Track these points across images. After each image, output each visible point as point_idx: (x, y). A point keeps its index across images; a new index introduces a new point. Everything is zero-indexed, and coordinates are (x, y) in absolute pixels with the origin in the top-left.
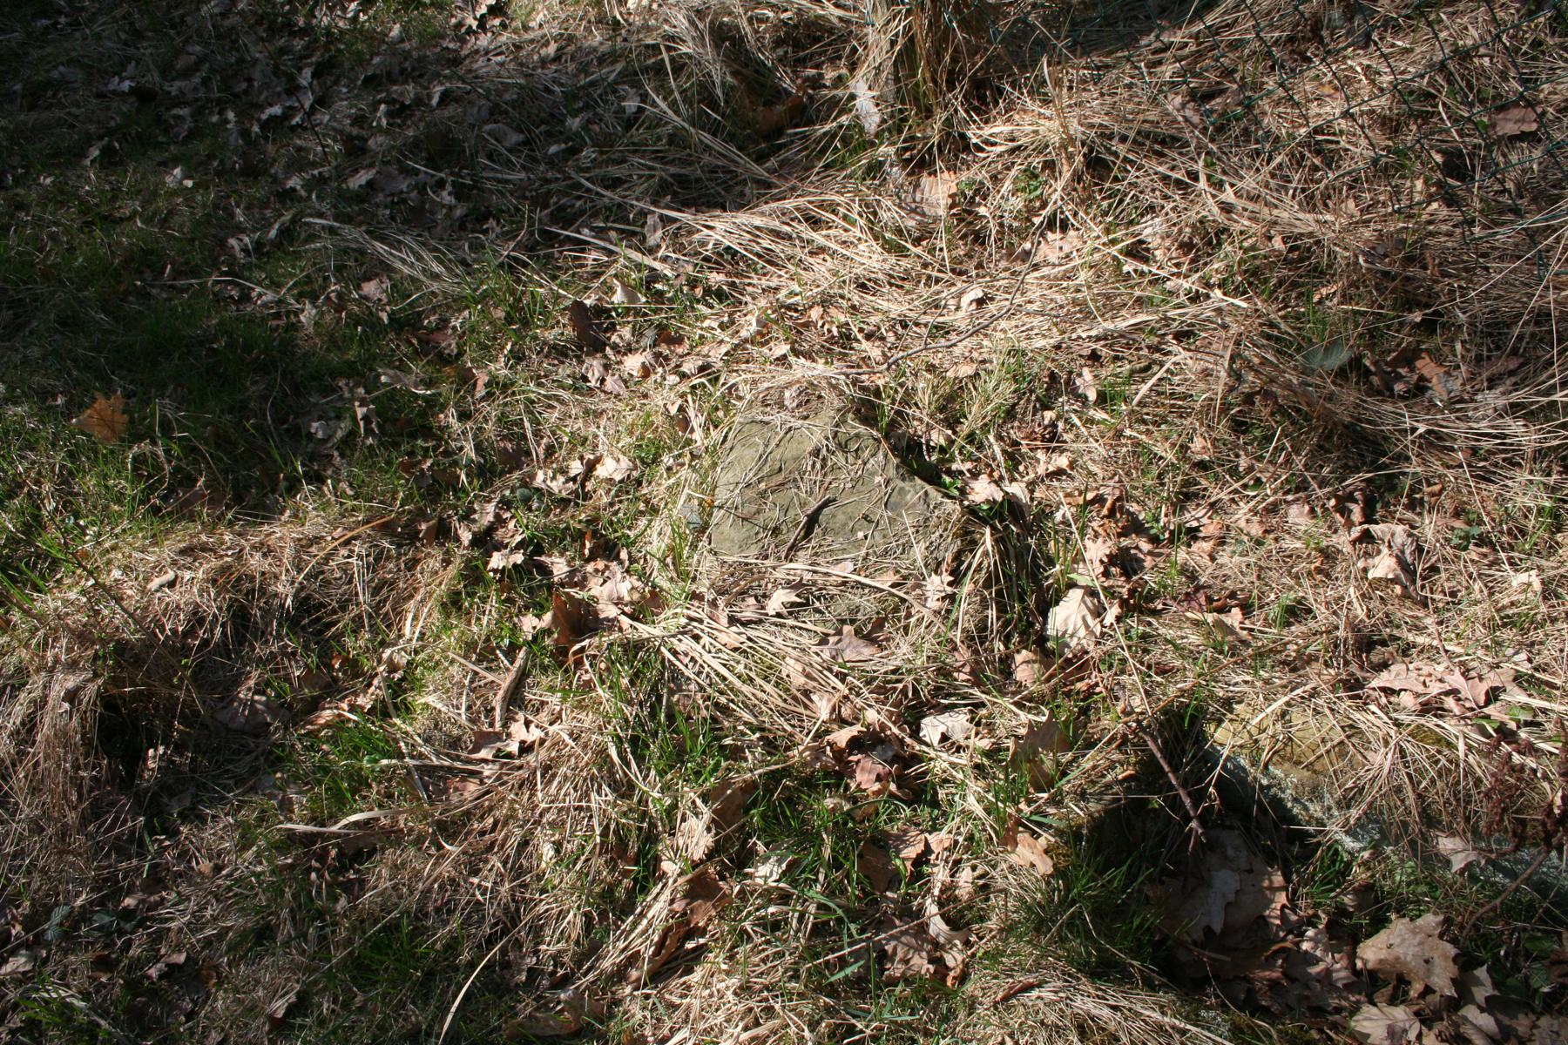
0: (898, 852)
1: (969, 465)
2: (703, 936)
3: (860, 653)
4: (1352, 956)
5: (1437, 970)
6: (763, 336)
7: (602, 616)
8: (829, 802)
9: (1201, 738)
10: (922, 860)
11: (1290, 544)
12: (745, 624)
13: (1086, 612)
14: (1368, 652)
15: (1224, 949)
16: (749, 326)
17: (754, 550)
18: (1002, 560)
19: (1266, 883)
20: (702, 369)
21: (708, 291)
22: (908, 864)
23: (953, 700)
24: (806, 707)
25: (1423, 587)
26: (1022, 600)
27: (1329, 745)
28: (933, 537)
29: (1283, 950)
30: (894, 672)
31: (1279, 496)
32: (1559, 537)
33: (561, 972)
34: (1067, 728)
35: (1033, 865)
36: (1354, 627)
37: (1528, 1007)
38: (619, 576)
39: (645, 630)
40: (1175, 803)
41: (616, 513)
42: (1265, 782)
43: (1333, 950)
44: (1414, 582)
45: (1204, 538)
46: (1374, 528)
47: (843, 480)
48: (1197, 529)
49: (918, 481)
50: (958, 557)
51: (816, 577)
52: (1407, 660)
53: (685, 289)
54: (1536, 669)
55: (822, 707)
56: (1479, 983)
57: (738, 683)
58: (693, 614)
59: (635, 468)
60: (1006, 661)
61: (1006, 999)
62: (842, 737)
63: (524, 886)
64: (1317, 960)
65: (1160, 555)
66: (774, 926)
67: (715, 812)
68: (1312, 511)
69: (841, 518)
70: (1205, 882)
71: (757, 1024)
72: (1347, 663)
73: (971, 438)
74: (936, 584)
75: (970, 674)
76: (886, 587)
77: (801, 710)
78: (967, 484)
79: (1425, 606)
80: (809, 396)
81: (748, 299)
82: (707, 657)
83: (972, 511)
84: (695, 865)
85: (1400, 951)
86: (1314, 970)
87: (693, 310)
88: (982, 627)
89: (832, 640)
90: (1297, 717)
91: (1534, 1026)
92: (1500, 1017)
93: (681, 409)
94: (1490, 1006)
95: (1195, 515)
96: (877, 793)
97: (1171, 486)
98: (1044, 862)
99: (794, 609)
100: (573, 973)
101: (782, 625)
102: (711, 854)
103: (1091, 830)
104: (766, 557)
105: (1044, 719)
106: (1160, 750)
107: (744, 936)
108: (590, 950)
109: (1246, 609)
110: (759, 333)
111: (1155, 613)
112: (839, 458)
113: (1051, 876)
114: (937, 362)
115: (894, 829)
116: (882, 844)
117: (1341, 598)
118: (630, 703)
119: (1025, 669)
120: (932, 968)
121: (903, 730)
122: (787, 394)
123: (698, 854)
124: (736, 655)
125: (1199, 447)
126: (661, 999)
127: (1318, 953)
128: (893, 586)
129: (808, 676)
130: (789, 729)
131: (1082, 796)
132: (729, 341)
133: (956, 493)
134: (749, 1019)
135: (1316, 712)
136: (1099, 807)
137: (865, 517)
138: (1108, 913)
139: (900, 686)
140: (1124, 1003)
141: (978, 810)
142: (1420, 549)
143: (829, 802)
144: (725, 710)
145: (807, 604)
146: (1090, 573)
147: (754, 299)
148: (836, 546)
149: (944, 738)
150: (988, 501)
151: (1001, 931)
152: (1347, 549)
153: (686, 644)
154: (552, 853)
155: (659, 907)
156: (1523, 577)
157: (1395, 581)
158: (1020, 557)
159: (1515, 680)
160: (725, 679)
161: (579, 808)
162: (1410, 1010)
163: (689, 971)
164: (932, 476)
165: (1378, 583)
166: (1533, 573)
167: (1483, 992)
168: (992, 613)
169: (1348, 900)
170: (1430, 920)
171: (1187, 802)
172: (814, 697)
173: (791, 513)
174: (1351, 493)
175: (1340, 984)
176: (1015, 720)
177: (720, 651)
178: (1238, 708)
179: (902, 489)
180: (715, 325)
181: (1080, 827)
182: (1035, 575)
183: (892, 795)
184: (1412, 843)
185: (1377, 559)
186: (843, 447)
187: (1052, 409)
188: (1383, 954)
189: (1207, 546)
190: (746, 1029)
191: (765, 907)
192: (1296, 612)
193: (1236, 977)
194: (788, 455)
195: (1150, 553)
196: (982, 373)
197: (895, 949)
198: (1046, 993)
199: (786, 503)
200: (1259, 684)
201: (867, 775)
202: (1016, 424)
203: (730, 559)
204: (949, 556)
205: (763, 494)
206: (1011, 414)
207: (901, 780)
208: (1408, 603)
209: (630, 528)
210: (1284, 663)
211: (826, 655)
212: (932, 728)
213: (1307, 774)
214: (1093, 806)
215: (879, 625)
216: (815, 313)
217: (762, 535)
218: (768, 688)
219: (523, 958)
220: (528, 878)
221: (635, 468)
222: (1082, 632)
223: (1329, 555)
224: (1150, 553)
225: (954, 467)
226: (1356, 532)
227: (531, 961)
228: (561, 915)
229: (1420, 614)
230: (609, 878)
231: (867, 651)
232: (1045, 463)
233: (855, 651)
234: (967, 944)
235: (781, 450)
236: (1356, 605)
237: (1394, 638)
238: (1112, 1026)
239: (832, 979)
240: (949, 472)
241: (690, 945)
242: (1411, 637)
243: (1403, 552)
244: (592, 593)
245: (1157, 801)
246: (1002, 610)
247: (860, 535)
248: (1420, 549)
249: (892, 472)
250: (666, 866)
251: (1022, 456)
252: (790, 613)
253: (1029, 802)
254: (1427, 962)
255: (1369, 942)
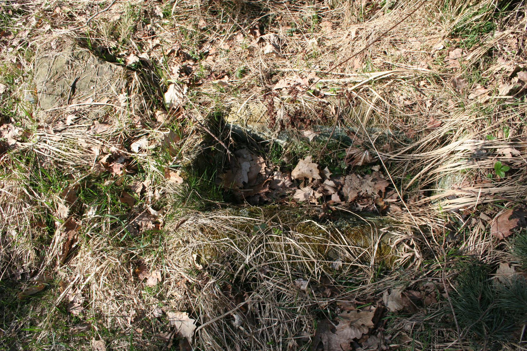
0: (135, 191)
1: (125, 52)
2: (76, 241)
3: (103, 129)
4: (290, 176)
5: (314, 173)
6: (40, 24)
7: (10, 144)
8: (107, 183)
9: (223, 122)
10: (143, 191)
11: (239, 49)
12: (60, 132)
13: (176, 91)
14: (271, 78)
15: (251, 187)
16: (34, 22)
17: (57, 104)
18: (143, 82)
19: (258, 162)
20: (20, 42)
21: (14, 12)
22: (139, 194)
23: (140, 135)
24: (91, 153)
25: (283, 52)
26: (154, 94)
27: (263, 113)
28: (117, 81)
29: (268, 181)
30: (116, 132)
31: (232, 34)
32: (321, 25)
33: (33, 271)
34: (178, 132)
35: (177, 182)
36: (265, 72)
37: (341, 175)
38: (14, 128)
39: (26, 145)
40: (220, 146)
41: (5, 106)
42: (248, 130)
43: (283, 176)
44: (279, 51)
45: (210, 55)
46: (263, 37)
47: (80, 70)
48: (208, 52)
49: (107, 62)
50: (127, 86)
51: (81, 107)
52: (284, 77)
53: (5, 13)
54: (322, 70)
55: (96, 151)
56: (327, 172)
57: (64, 153)
58: (41, 134)
59: (7, 87)
60: (153, 116)
61: (177, 227)
62: (104, 160)
63: (9, 247)
64: (280, 181)
65: (197, 65)
66: (98, 230)
67: (66, 199)
68: (244, 36)
69: (83, 84)
70: (239, 168)
71: (101, 264)
72: (265, 84)
73: (124, 42)
74: (122, 97)
75: (141, 124)
76: (105, 103)
77: (89, 155)
78: (126, 59)
79: (285, 58)
80: (60, 43)
81: (32, 11)
82: (50, 147)
83: (129, 68)
84: (66, 219)
85: (302, 170)
86: (279, 184)
87: (11, 20)
88: (142, 107)
89: (92, 127)
90: (251, 106)
91: (345, 180)
92: (335, 180)
93: (17, 60)
94: (331, 178)
95: (206, 47)
96: (122, 174)
97: (195, 41)
98: (180, 180)
99: (76, 121)
100: (38, 270)
101: (74, 128)
102: (70, 214)
103: (194, 164)
104: (61, 106)
105: (169, 132)
106: (210, 131)
107: (89, 237)
108: (40, 258)
109: (228, 75)
110: (38, 23)
111: (200, 85)
112: (77, 62)
113: (183, 183)
114: (106, 17)
115: (132, 184)
116: (130, 190)
117: (258, 63)
118: (27, 172)
119: (161, 117)
120: (154, 225)
121: (125, 151)
122: (52, 44)
123: (66, 215)
124: (60, 143)
125: (202, 23)
126: (70, 267)
127: (279, 179)
128: (107, 102)
129: (87, 142)
130: (87, 162)
131: (188, 153)
132: (28, 29)
133: (122, 63)
134: (98, 263)
135: (257, 103)
136: (195, 155)
137: (92, 81)
138: (204, 190)
139: (119, 136)
140: (215, 216)
141: (155, 169)
142: (279, 40)
143: (107, 183)
144: (63, 163)
145: (80, 117)
146: (174, 78)
147: (34, 10)
148: (84, 94)
149: (139, 148)
150: (134, 63)
151: (172, 206)
152: (257, 46)
153: (42, 145)
154: (16, 233)
155: (59, 237)
156: (311, 41)
157: (273, 52)
158: (150, 79)
159: (316, 75)
160: (59, 153)
161: (20, 215)
162: (310, 187)
163: (76, 254)
164: (113, 60)
165: (268, 55)
166: (314, 38)
167: (328, 175)
168: (144, 101)
169: (285, 159)
170: (308, 158)
171: (223, 144)
172: (92, 149)
173: (66, 87)
174: (255, 26)
175: (288, 186)
176: (159, 135)
177: (54, 143)
178: (232, 109)
179: (102, 67)
180: (21, 24)
181: (190, 164)
182: (156, 84)
183: (127, 173)
184: (296, 136)
185: (266, 47)
186: (77, 58)
187: (149, 24)
188: (298, 173)
189: (211, 57)
190: (98, 266)
191: (93, 225)
192: (244, 73)
193: (255, 195)
194: (58, 66)
195: (194, 65)
196: (122, 17)
197: (141, 223)
198: (189, 222)
199: (62, 84)
200: (237, 99)
201: (117, 169)
202: (139, 32)
203: (49, 110)
204: (124, 86)
205: (53, 83)
206: (135, 29)
207: (128, 167)
208: (280, 59)
209: (12, 110)
210: (245, 90)
211: (92, 133)
212: (135, 147)
213: (259, 124)
214: (193, 156)
215: (107, 116)
216: (58, 10)
217: (58, 98)
218: (75, 151)
219: (18, 271)
220: (10, 244)
221: (7, 87)
222: (176, 98)
223: (251, 50)
224: (194, 65)
225: (120, 54)
226: (258, 39)
227: (21, 271)
228: (27, 252)
229: (284, 61)
230: (40, 234)
231: (105, 127)
232: (151, 44)
233: (101, 129)
234: (164, 214)
235: (55, 65)
236: (263, 63)
237: (278, 72)
238: (211, 225)
239: (121, 240)
240: (119, 56)
241: (74, 246)
242: (283, 70)
243: (274, 42)
244: (5, 137)
245: (213, 148)
246: (147, 99)
247: (92, 88)
248: (279, 40)
249: (97, 62)
250: (57, 223)
251: (143, 43)
252: (75, 123)
253: (172, 161)
254: (311, 171)
255: (294, 170)
